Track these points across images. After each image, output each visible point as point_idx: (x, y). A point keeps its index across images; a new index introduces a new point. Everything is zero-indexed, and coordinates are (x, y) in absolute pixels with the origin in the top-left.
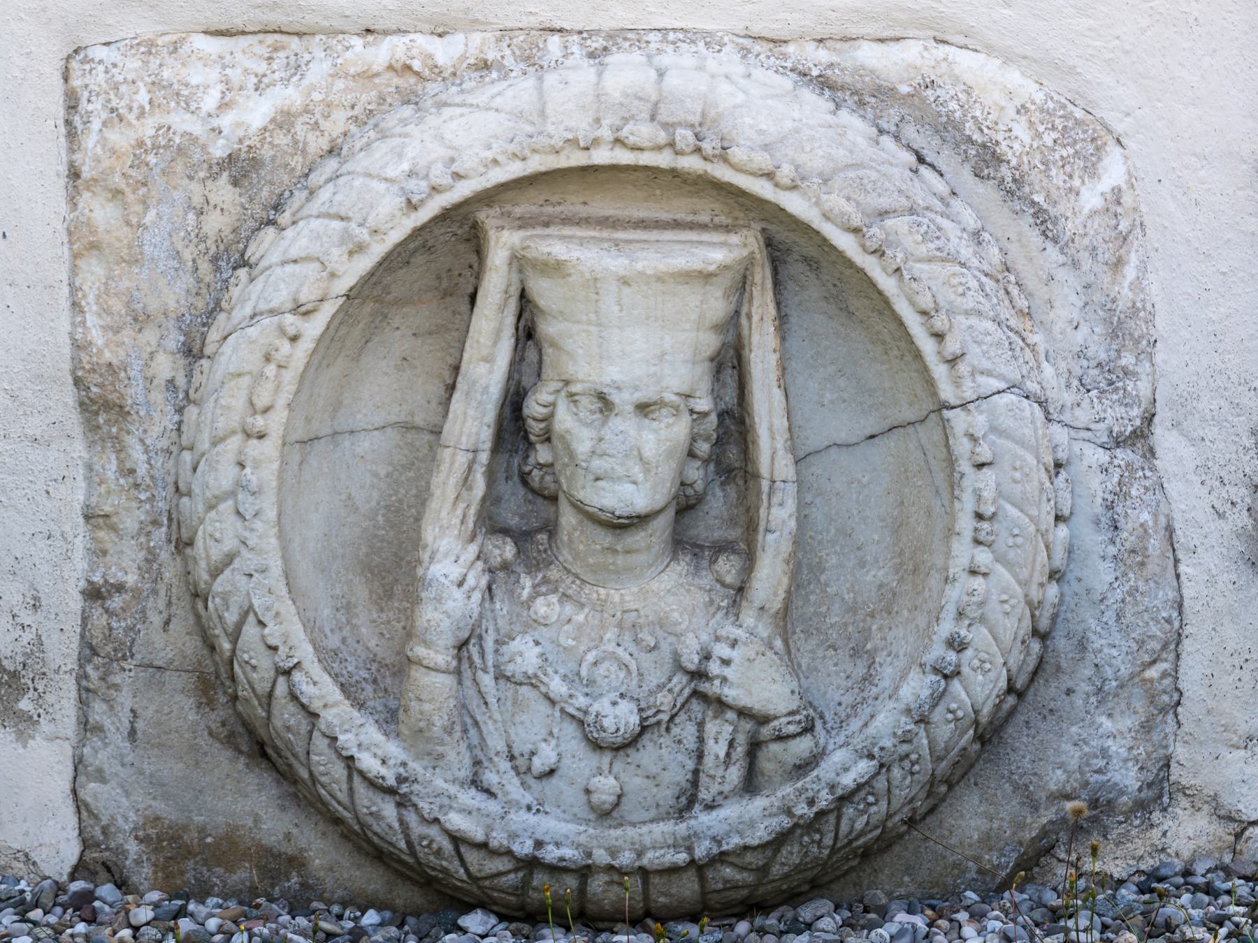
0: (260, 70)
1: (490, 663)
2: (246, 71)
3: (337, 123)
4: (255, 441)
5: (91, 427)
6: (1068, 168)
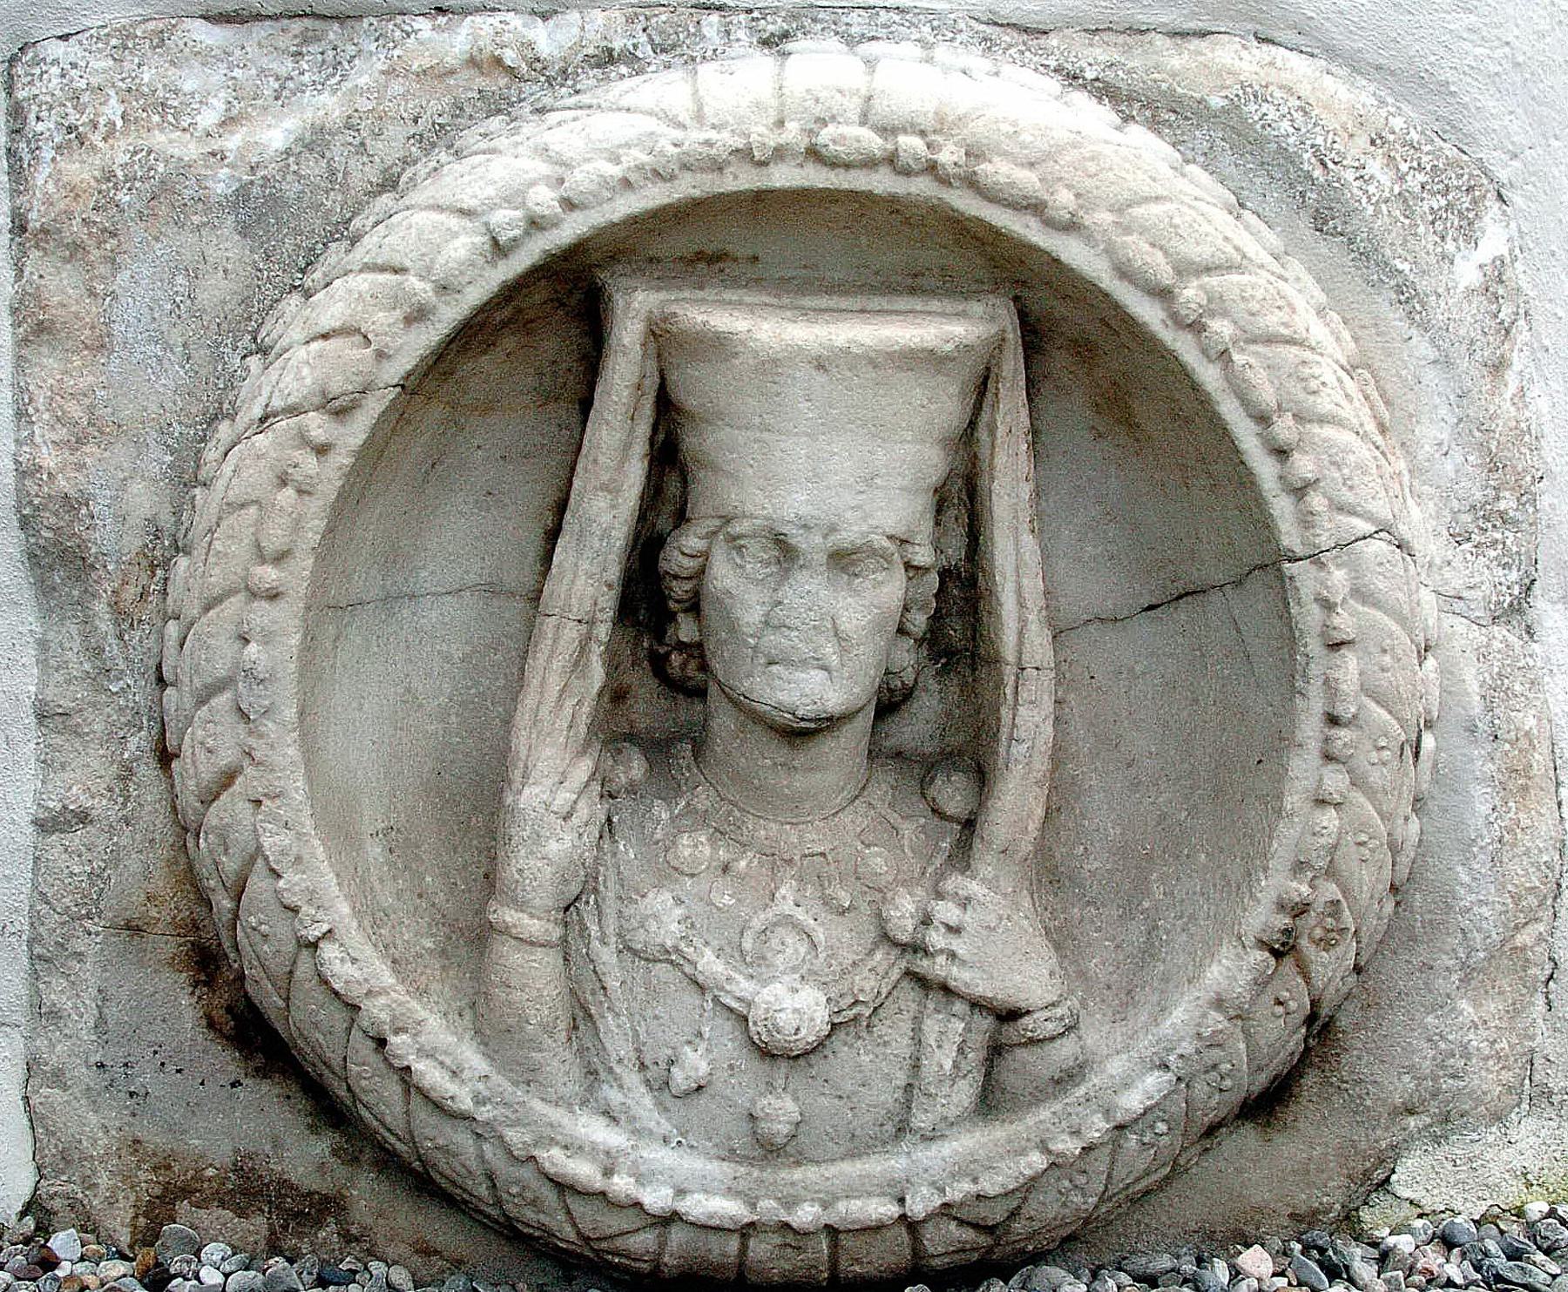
0: (283, 72)
1: (611, 930)
2: (262, 72)
3: (391, 146)
4: (265, 604)
5: (44, 589)
6: (1439, 226)
